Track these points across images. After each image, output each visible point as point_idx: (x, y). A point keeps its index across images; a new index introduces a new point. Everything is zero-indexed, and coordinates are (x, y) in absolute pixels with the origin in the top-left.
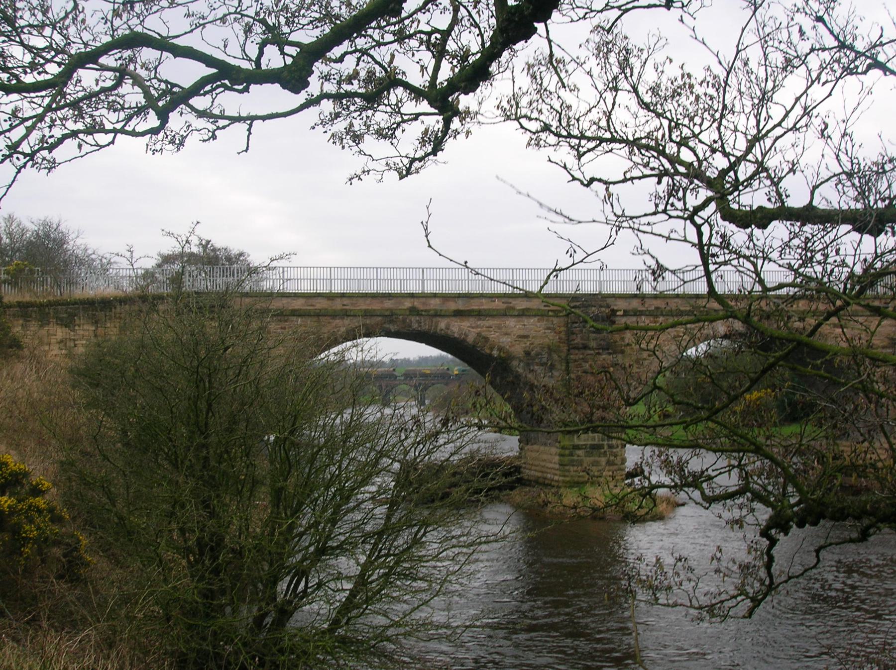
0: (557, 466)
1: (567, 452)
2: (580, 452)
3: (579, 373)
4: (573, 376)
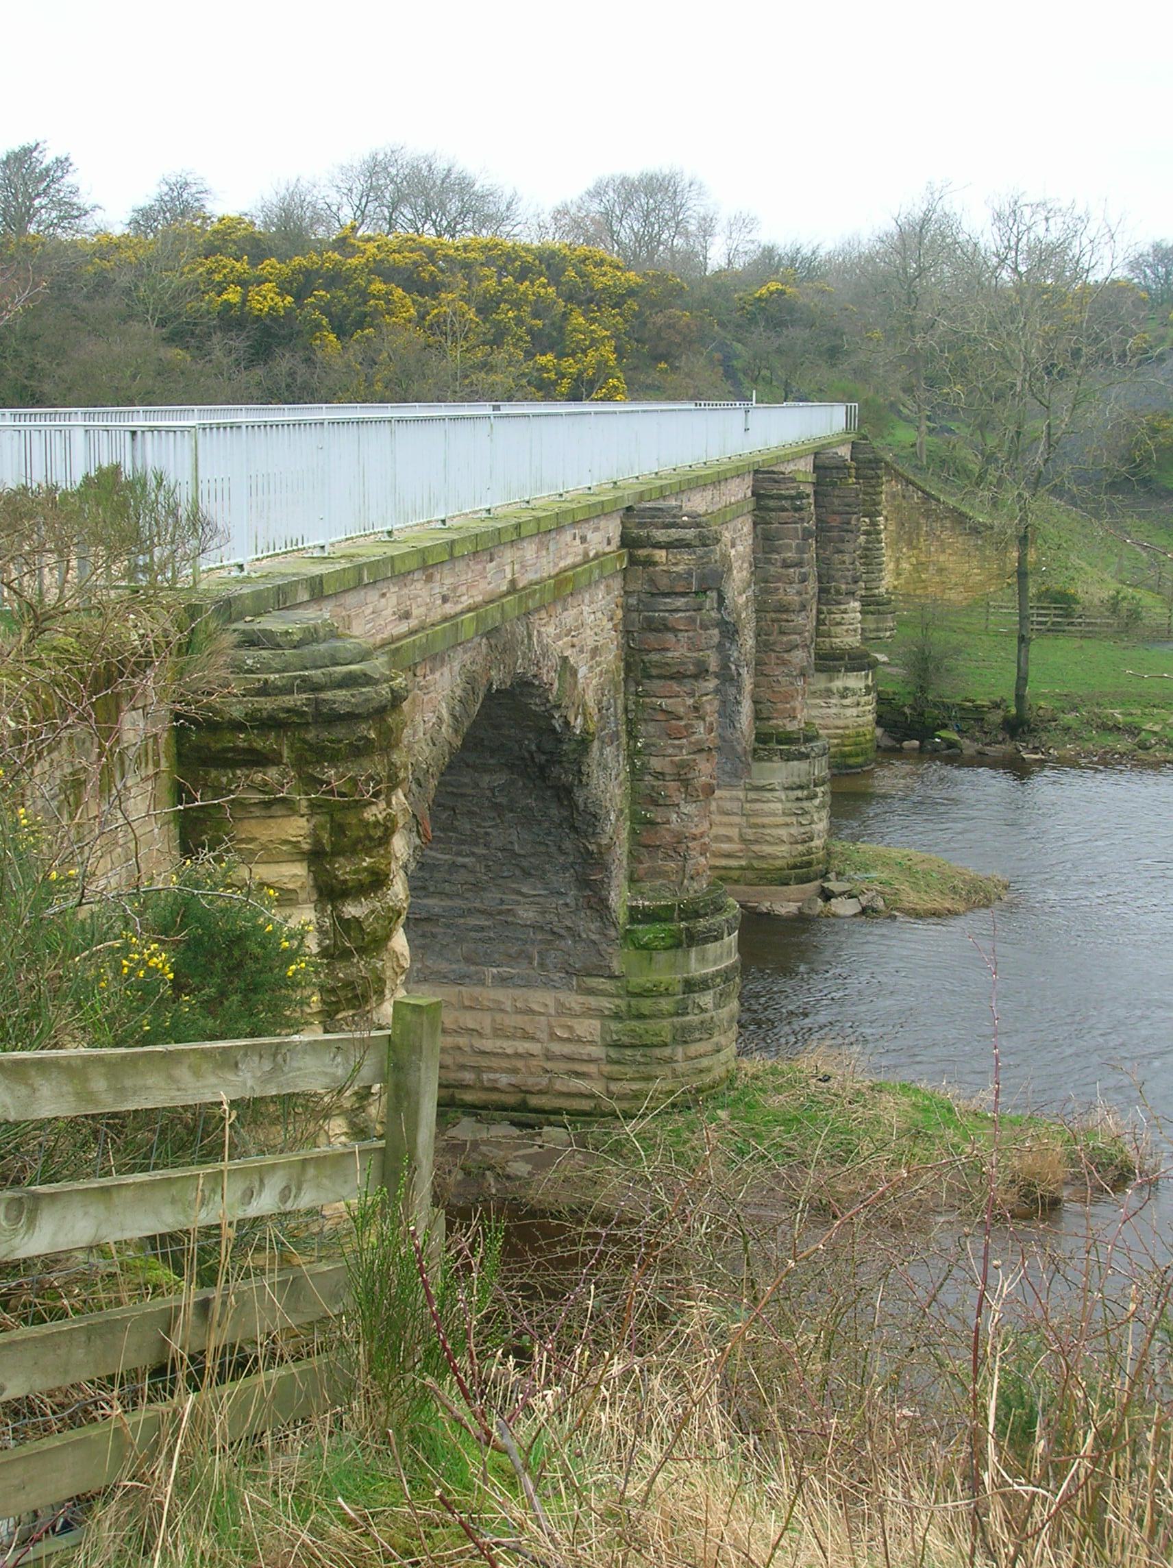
0: (598, 1051)
1: (666, 1004)
2: (707, 999)
3: (685, 756)
4: (656, 763)
